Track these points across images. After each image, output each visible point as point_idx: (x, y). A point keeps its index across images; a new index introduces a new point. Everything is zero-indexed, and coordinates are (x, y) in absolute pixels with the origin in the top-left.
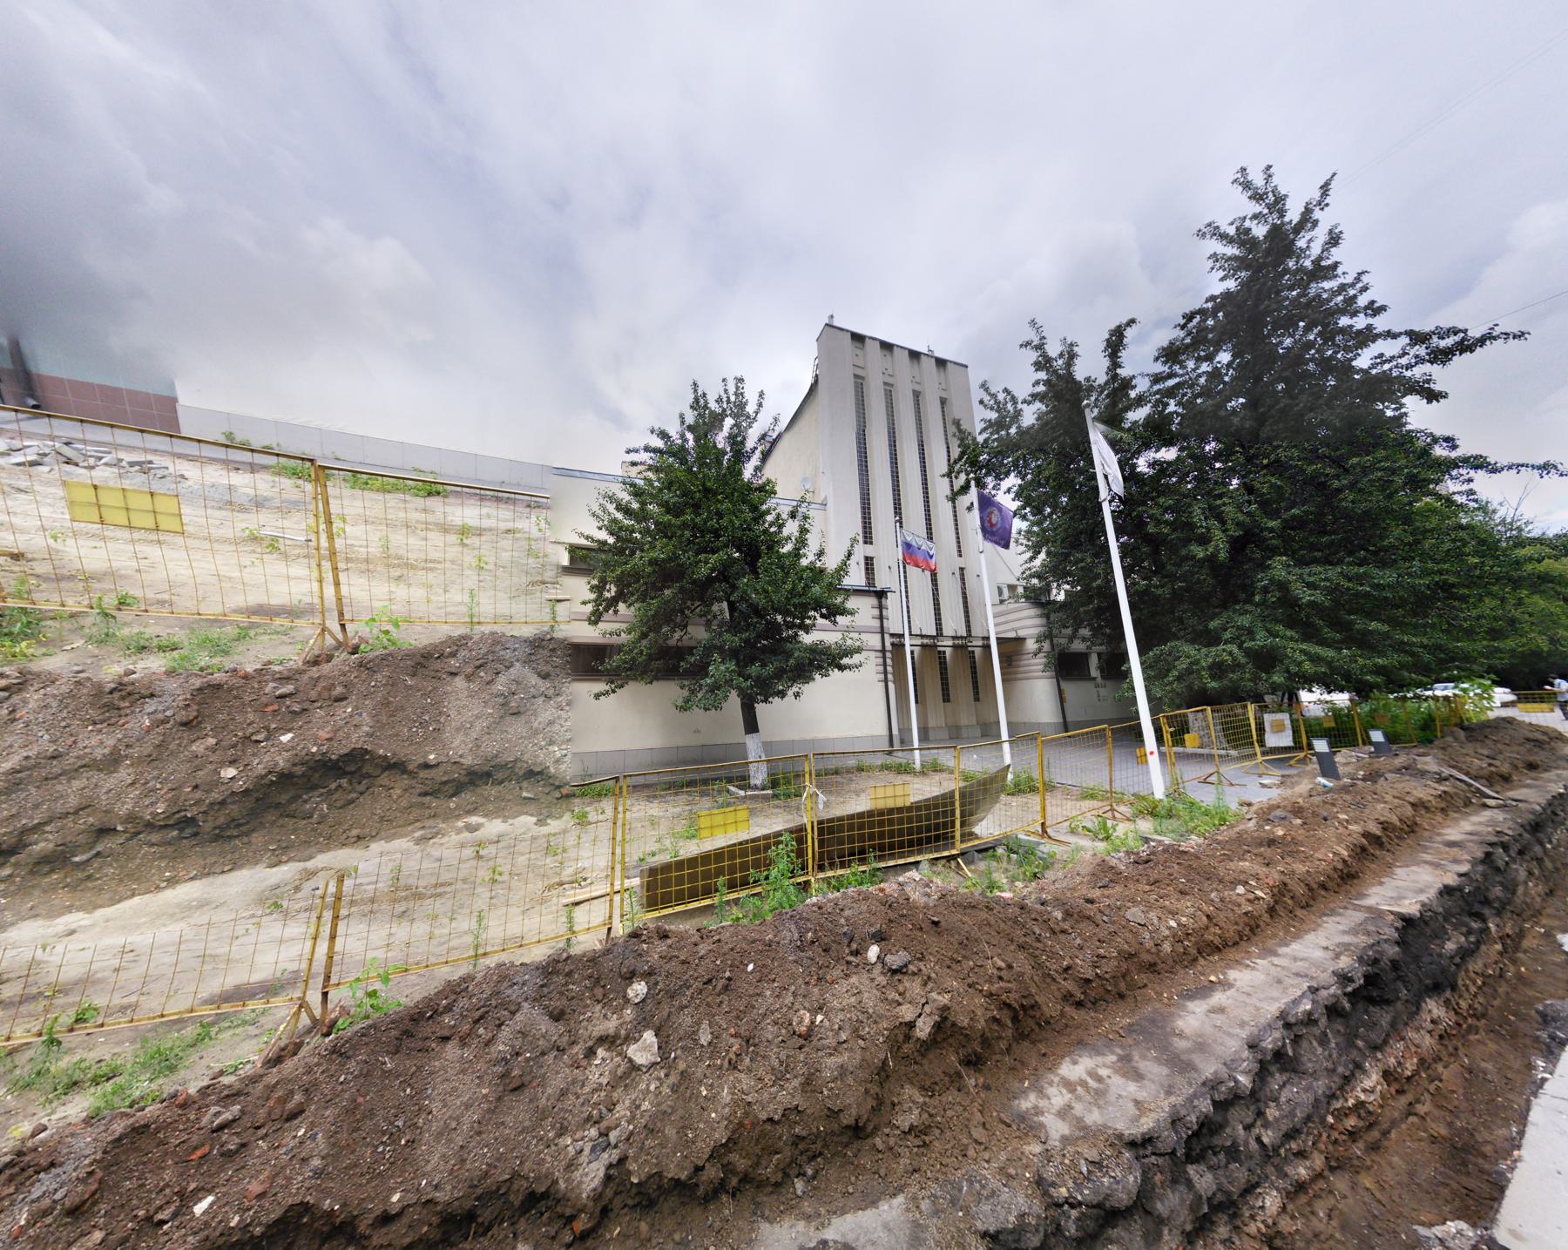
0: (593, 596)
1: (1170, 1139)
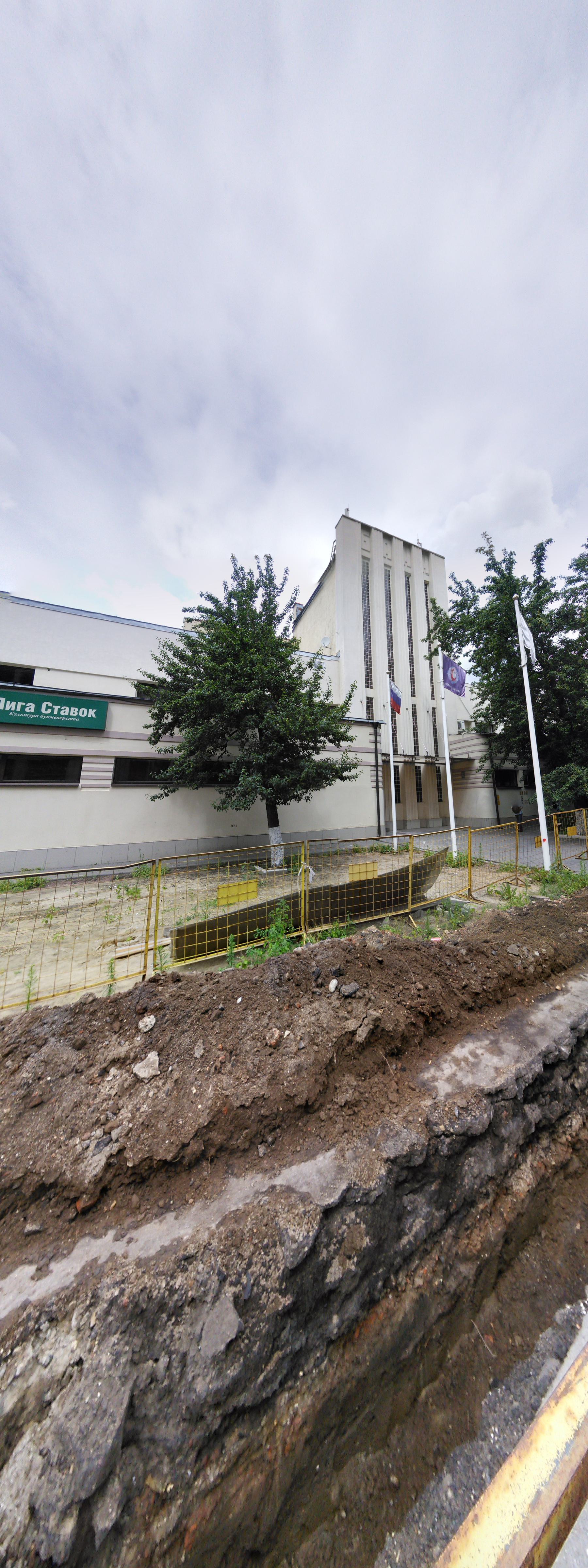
0: (154, 722)
1: (514, 1089)
